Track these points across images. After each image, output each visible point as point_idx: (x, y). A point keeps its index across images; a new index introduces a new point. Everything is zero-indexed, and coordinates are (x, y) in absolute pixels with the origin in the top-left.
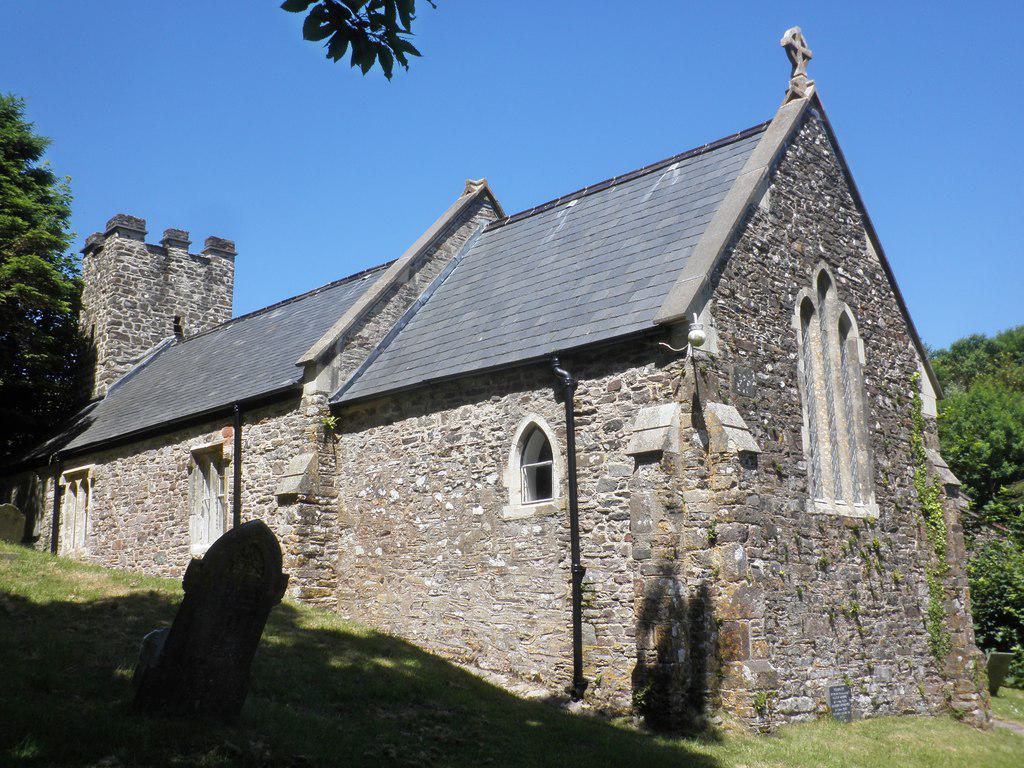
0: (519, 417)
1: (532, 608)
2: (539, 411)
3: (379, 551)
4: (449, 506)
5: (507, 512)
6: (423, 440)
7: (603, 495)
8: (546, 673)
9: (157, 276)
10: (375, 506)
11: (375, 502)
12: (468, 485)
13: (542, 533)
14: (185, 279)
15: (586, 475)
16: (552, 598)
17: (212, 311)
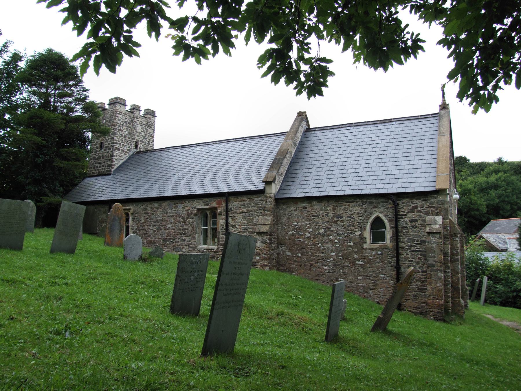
0: (371, 213)
1: (376, 279)
2: (381, 213)
3: (299, 255)
4: (336, 241)
5: (365, 246)
6: (323, 216)
7: (409, 244)
8: (382, 301)
9: (129, 123)
10: (297, 238)
11: (297, 236)
12: (346, 234)
13: (382, 254)
14: (139, 126)
15: (401, 236)
16: (385, 276)
17: (148, 140)
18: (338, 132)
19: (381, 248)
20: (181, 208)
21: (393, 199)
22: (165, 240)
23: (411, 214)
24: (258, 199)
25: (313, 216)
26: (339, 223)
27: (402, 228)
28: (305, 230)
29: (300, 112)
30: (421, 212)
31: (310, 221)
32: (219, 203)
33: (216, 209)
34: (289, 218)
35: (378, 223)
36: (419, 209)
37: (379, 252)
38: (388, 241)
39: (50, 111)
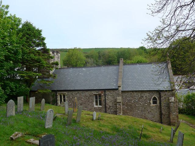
0: (153, 96)
20: (87, 93)
24: (116, 91)
28: (131, 101)
35: (155, 98)
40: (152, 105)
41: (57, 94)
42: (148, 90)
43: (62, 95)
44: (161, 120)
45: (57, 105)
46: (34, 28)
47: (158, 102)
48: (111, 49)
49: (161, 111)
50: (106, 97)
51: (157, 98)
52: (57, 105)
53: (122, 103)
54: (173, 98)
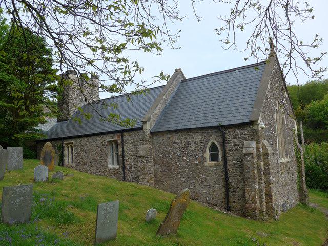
0: (209, 140)
3: (167, 170)
5: (206, 164)
18: (199, 82)
19: (216, 165)
20: (99, 140)
21: (221, 129)
22: (92, 162)
23: (234, 140)
24: (140, 133)
25: (173, 143)
26: (189, 148)
27: (229, 150)
28: (169, 154)
29: (24, 157)
30: (241, 138)
31: (171, 147)
32: (118, 137)
33: (117, 141)
34: (159, 146)
35: (213, 148)
36: (239, 136)
37: (215, 168)
38: (220, 161)
39: (33, 149)
40: (208, 162)
41: (64, 145)
42: (199, 126)
43: (69, 146)
44: (228, 202)
45: (63, 165)
46: (304, 87)
47: (220, 156)
48: (254, 73)
49: (227, 180)
50: (125, 147)
51: (218, 146)
52: (63, 165)
53: (154, 159)
54: (254, 144)
